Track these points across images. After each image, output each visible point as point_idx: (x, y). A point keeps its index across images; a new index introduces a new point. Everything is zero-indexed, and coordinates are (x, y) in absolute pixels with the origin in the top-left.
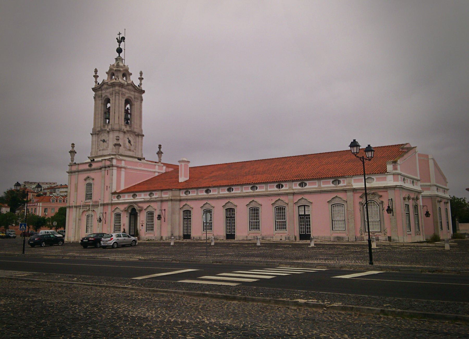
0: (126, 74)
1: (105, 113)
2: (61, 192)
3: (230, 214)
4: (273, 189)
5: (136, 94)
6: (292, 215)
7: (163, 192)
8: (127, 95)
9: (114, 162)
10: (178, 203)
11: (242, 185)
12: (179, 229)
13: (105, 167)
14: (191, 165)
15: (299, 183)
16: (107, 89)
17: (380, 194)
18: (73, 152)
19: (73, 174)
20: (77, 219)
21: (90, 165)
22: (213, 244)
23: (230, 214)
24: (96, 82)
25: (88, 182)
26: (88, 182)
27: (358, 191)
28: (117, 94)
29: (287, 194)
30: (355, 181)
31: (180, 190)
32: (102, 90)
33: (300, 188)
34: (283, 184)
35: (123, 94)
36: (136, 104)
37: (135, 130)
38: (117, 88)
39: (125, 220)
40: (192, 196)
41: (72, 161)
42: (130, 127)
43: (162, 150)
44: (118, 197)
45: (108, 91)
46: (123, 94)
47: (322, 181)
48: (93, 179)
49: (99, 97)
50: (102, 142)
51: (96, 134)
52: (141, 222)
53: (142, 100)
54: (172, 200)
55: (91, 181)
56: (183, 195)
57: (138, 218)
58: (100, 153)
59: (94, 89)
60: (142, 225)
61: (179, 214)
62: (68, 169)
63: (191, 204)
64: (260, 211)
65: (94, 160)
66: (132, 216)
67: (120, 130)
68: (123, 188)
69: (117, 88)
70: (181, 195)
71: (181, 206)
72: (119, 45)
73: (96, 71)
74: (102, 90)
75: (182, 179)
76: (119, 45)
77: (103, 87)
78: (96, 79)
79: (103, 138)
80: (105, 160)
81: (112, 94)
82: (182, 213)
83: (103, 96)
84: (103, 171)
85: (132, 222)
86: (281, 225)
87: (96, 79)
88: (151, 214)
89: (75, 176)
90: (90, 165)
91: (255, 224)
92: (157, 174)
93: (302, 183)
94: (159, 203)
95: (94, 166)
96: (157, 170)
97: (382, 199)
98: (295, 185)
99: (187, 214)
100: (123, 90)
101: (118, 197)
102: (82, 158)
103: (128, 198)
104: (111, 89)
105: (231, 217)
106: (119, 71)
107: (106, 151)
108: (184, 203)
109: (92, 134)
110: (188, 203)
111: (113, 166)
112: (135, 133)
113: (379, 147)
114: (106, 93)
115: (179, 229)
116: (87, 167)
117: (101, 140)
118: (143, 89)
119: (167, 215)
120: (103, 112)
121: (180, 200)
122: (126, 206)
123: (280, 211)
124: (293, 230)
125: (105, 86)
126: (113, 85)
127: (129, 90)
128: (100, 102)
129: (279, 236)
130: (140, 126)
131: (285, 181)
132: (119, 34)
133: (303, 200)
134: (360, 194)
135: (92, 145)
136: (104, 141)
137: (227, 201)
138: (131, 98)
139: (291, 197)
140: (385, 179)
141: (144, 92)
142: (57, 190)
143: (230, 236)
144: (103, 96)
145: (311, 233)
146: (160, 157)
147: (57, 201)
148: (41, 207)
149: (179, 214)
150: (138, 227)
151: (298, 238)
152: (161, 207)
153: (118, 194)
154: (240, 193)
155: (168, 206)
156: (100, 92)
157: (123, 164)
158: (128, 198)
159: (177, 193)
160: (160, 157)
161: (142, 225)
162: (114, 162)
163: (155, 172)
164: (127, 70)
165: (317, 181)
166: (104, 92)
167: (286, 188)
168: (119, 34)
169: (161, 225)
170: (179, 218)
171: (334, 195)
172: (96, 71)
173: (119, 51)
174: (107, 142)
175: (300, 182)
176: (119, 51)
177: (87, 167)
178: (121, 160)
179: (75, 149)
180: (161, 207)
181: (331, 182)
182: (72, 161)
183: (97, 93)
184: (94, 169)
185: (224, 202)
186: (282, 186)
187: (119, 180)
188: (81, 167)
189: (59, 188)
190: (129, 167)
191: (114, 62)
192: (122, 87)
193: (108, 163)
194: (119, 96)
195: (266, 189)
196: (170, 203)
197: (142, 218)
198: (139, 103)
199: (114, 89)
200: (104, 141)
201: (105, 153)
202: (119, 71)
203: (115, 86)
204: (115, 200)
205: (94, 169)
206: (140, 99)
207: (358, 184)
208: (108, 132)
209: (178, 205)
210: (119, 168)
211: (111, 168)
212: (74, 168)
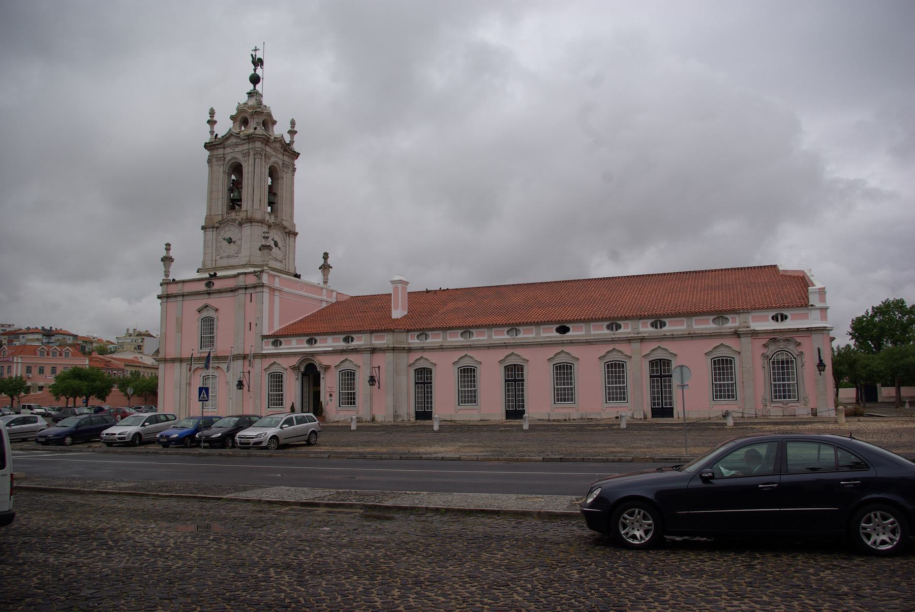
0: (268, 122)
1: (231, 190)
2: (28, 340)
3: (514, 377)
4: (601, 331)
5: (286, 158)
6: (638, 376)
7: (374, 335)
8: (273, 159)
9: (265, 279)
10: (405, 355)
11: (538, 324)
12: (408, 403)
13: (246, 288)
14: (410, 289)
15: (343, 336)
16: (237, 145)
17: (799, 340)
18: (167, 260)
19: (172, 299)
20: (184, 382)
21: (209, 284)
22: (354, 427)
23: (514, 377)
24: (212, 132)
25: (205, 314)
26: (205, 314)
27: (760, 336)
28: (259, 156)
29: (629, 340)
30: (755, 319)
31: (408, 331)
32: (224, 148)
33: (653, 329)
34: (354, 336)
35: (267, 157)
36: (286, 177)
37: (285, 223)
38: (258, 144)
39: (293, 389)
40: (522, 338)
41: (167, 275)
42: (276, 217)
43: (329, 261)
44: (276, 343)
45: (240, 148)
46: (267, 157)
47: (694, 318)
48: (217, 310)
49: (218, 159)
50: (226, 242)
51: (213, 227)
52: (329, 390)
53: (294, 170)
54: (394, 349)
55: (211, 314)
56: (414, 341)
57: (322, 382)
58: (225, 262)
59: (207, 146)
60: (331, 395)
61: (408, 374)
62: (159, 291)
63: (432, 357)
64: (478, 373)
65: (215, 274)
66: (306, 379)
67: (262, 222)
68: (277, 328)
69: (258, 144)
70: (410, 341)
71: (412, 361)
72: (255, 70)
73: (212, 113)
74: (224, 148)
75: (398, 313)
76: (255, 70)
77: (229, 142)
78: (212, 127)
79: (227, 236)
80: (245, 274)
81: (246, 154)
82: (412, 373)
83: (228, 158)
84: (241, 296)
85: (305, 390)
86: (616, 393)
87: (212, 127)
88: (349, 377)
89: (174, 304)
90: (209, 284)
91: (564, 394)
92: (324, 305)
93: (612, 324)
94: (367, 356)
95: (218, 285)
96: (324, 298)
97: (800, 349)
98: (644, 325)
99: (424, 378)
100: (268, 149)
101: (276, 343)
102: (186, 271)
103: (298, 346)
104: (246, 147)
105: (515, 381)
106: (253, 116)
107: (237, 259)
108: (417, 355)
109: (203, 228)
110: (426, 355)
111: (263, 286)
112: (285, 228)
113: (640, 276)
114: (232, 153)
115: (408, 403)
116: (202, 287)
117: (224, 239)
118: (297, 150)
119: (385, 378)
120: (226, 189)
121: (410, 350)
122: (294, 361)
123: (615, 370)
124: (638, 402)
125: (233, 140)
126: (250, 138)
127: (275, 149)
128: (221, 169)
129: (608, 411)
130: (292, 217)
131: (626, 318)
132: (256, 50)
133: (467, 359)
134: (765, 341)
135: (205, 247)
136: (230, 241)
137: (611, 347)
138: (278, 164)
139: (636, 346)
140: (806, 317)
141: (297, 155)
142: (21, 336)
143: (515, 413)
144: (228, 158)
145: (525, 408)
146: (325, 276)
147: (48, 354)
148: (20, 365)
149: (408, 374)
150: (322, 399)
151: (649, 415)
152: (371, 363)
153: (276, 339)
154: (533, 338)
155: (384, 361)
156: (221, 151)
157: (277, 284)
158: (298, 346)
159: (402, 337)
160: (325, 276)
161: (331, 395)
162: (265, 279)
163: (322, 301)
164: (270, 115)
165: (684, 319)
166: (228, 150)
167: (626, 329)
168: (256, 50)
169: (371, 395)
170: (408, 381)
171: (717, 342)
172: (212, 113)
173: (255, 80)
174: (238, 242)
175: (608, 323)
176: (255, 80)
177: (202, 287)
178: (274, 276)
179: (172, 253)
180: (371, 363)
181: (770, 318)
182: (167, 275)
183: (215, 152)
184: (220, 292)
185: (502, 354)
186: (352, 340)
187: (271, 313)
188: (188, 288)
189: (25, 333)
190: (286, 289)
191: (244, 99)
192: (266, 145)
193: (252, 280)
194: (251, 161)
195: (490, 336)
196: (389, 356)
197: (330, 384)
198: (289, 175)
199: (251, 146)
200: (230, 241)
201: (233, 262)
202: (253, 116)
203: (254, 142)
204: (269, 349)
205: (220, 292)
206: (291, 168)
207: (764, 323)
208: (241, 224)
209: (405, 360)
210: (273, 290)
211: (259, 290)
212: (173, 289)
